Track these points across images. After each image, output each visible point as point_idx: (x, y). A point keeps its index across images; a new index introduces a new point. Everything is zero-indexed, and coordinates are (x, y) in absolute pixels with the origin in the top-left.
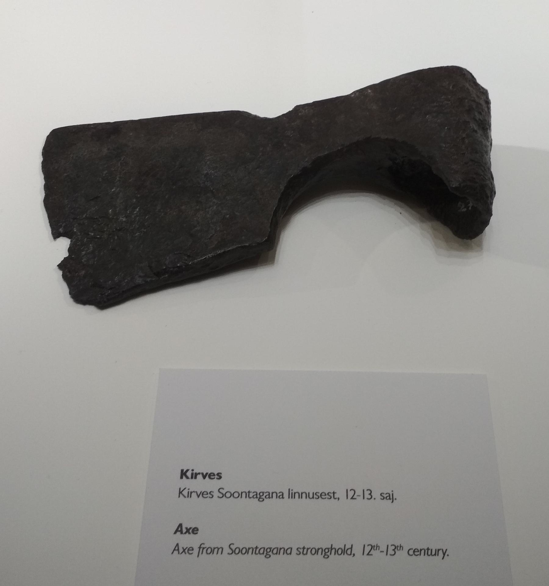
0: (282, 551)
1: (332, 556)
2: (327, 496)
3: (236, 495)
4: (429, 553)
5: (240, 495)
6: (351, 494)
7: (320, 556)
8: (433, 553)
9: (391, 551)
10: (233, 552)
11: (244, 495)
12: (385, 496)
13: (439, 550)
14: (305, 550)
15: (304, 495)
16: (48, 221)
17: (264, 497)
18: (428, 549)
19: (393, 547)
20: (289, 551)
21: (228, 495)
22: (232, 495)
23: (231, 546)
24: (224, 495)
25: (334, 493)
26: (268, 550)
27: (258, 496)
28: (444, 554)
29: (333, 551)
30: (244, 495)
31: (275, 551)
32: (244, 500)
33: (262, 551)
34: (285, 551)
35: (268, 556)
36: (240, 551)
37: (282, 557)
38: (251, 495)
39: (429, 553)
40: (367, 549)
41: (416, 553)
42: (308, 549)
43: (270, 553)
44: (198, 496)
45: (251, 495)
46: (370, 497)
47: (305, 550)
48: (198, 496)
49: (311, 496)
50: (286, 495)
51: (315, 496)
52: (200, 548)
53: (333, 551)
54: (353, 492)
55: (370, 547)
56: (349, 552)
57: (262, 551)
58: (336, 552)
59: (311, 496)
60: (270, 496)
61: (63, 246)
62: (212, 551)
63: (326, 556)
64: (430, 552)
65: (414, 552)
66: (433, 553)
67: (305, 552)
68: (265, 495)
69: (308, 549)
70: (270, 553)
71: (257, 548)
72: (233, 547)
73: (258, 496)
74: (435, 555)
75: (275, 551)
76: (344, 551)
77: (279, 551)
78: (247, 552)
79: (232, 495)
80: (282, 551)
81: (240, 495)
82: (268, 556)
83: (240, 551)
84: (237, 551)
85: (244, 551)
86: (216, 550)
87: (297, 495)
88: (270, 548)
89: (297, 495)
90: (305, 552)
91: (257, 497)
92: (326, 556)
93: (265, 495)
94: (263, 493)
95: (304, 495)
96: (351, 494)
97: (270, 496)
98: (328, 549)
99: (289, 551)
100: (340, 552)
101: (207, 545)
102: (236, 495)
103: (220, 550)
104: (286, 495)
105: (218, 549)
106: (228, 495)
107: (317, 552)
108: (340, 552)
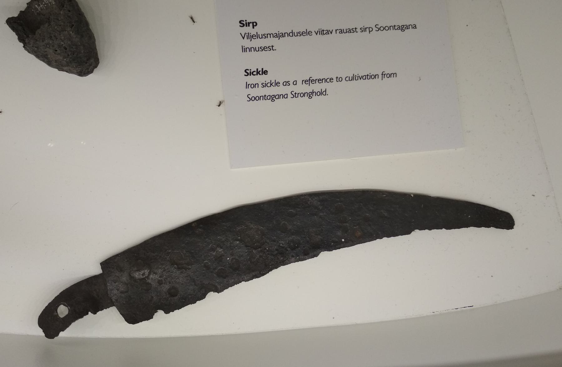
0: (281, 96)
1: (314, 97)
3: (387, 28)
5: (389, 28)
7: (306, 98)
10: (251, 99)
15: (252, 49)
16: (50, 301)
20: (286, 96)
24: (379, 29)
25: (272, 46)
31: (277, 97)
32: (392, 31)
33: (269, 98)
34: (283, 97)
35: (273, 100)
36: (255, 98)
37: (281, 100)
38: (396, 28)
44: (317, 34)
45: (396, 28)
48: (317, 34)
49: (257, 50)
56: (324, 93)
57: (269, 98)
58: (316, 94)
59: (257, 50)
60: (408, 27)
61: (160, 313)
63: (310, 97)
71: (265, 96)
72: (250, 97)
75: (277, 97)
76: (321, 93)
77: (279, 96)
78: (259, 98)
80: (281, 96)
81: (389, 28)
82: (273, 100)
83: (255, 98)
87: (248, 49)
89: (248, 49)
92: (310, 97)
95: (252, 49)
97: (408, 27)
99: (286, 96)
100: (318, 94)
102: (387, 28)
106: (382, 29)
107: (304, 95)
108: (318, 94)
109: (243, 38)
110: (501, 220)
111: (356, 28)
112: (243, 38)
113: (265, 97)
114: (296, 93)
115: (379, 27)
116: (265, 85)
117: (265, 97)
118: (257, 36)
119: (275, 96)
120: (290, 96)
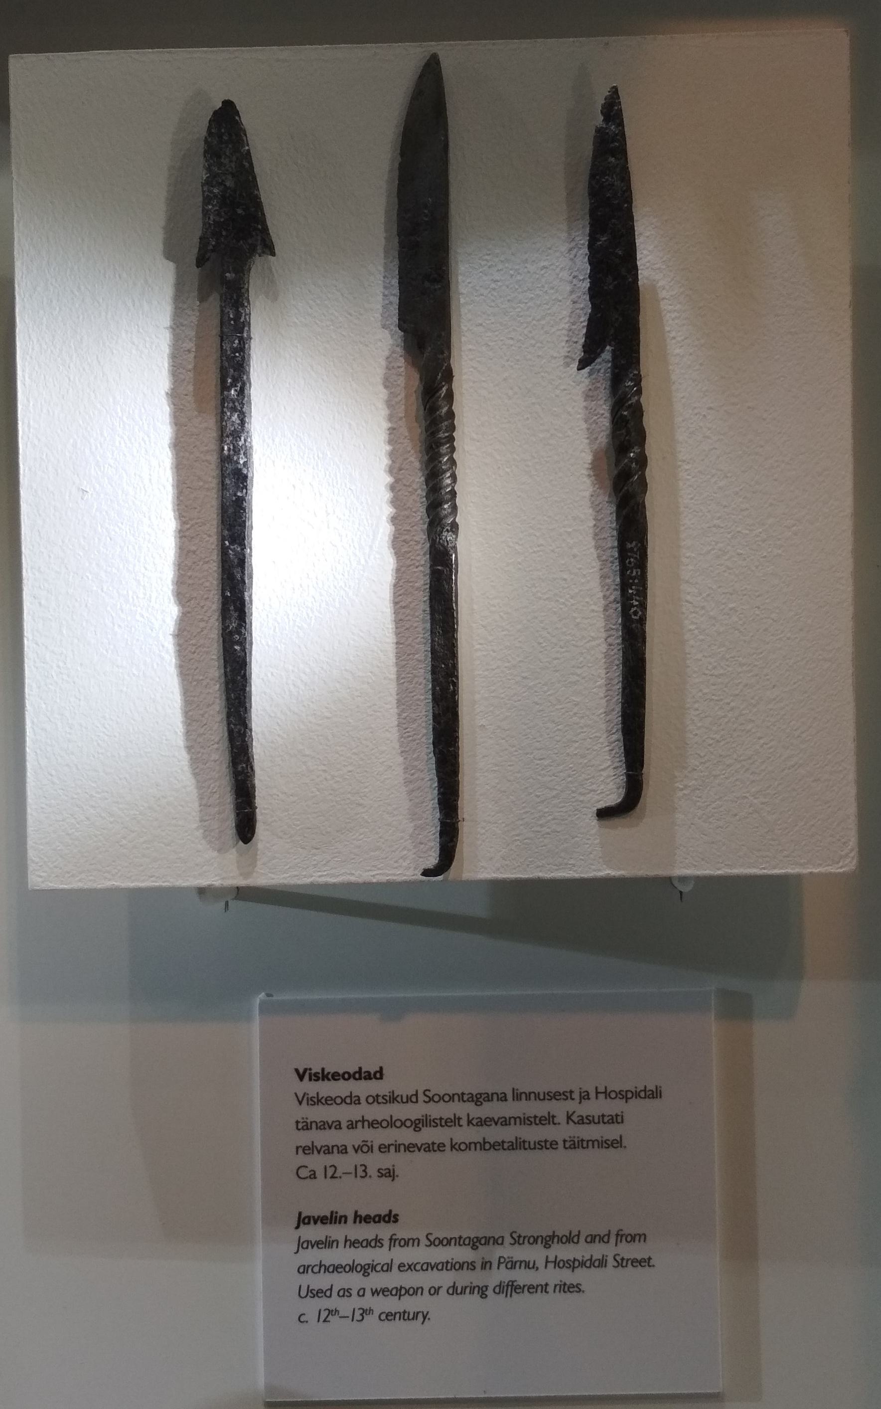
0: (598, 1238)
2: (563, 1097)
4: (406, 1317)
5: (452, 1098)
6: (330, 1172)
7: (539, 1246)
8: (411, 1317)
9: (358, 1316)
11: (456, 1098)
12: (384, 1172)
13: (418, 1313)
14: (521, 1239)
15: (532, 1096)
17: (481, 1100)
18: (405, 1312)
19: (361, 1311)
20: (500, 1242)
21: (436, 1098)
22: (442, 1098)
23: (429, 1237)
24: (431, 1099)
26: (475, 1240)
27: (475, 1099)
28: (424, 1318)
29: (556, 1240)
30: (456, 1098)
31: (483, 1241)
34: (601, 1239)
38: (606, 1120)
39: (406, 1317)
40: (324, 1315)
41: (389, 1318)
42: (525, 1237)
43: (478, 1244)
45: (606, 1120)
46: (363, 1174)
47: (521, 1239)
50: (510, 1096)
51: (547, 1097)
52: (391, 1239)
53: (556, 1240)
54: (333, 1169)
55: (327, 1312)
57: (467, 1242)
58: (560, 1240)
59: (542, 1097)
62: (633, 1239)
64: (406, 1315)
65: (387, 1316)
66: (411, 1317)
67: (521, 1242)
68: (483, 1096)
69: (525, 1237)
70: (478, 1244)
71: (460, 1238)
72: (432, 1238)
73: (475, 1099)
74: (413, 1319)
75: (483, 1241)
79: (442, 1098)
80: (598, 1238)
81: (452, 1098)
83: (441, 1242)
84: (437, 1242)
85: (445, 1242)
86: (637, 1238)
87: (523, 1096)
88: (477, 1238)
89: (523, 1096)
90: (521, 1242)
91: (473, 1101)
93: (483, 1096)
94: (480, 1094)
95: (532, 1096)
96: (330, 1172)
98: (549, 1236)
99: (500, 1242)
100: (564, 1240)
101: (626, 1232)
102: (447, 1098)
103: (643, 1237)
104: (510, 1096)
105: (414, 1240)
106: (436, 1098)
107: (536, 1241)
108: (564, 1240)
109: (300, 1103)
110: (655, 1094)
111: (571, 1092)
112: (300, 1103)
113: (335, 1076)
114: (519, 1237)
115: (430, 1094)
116: (376, 1099)
117: (335, 1076)
118: (393, 1099)
119: (479, 1239)
120: (611, 1262)
